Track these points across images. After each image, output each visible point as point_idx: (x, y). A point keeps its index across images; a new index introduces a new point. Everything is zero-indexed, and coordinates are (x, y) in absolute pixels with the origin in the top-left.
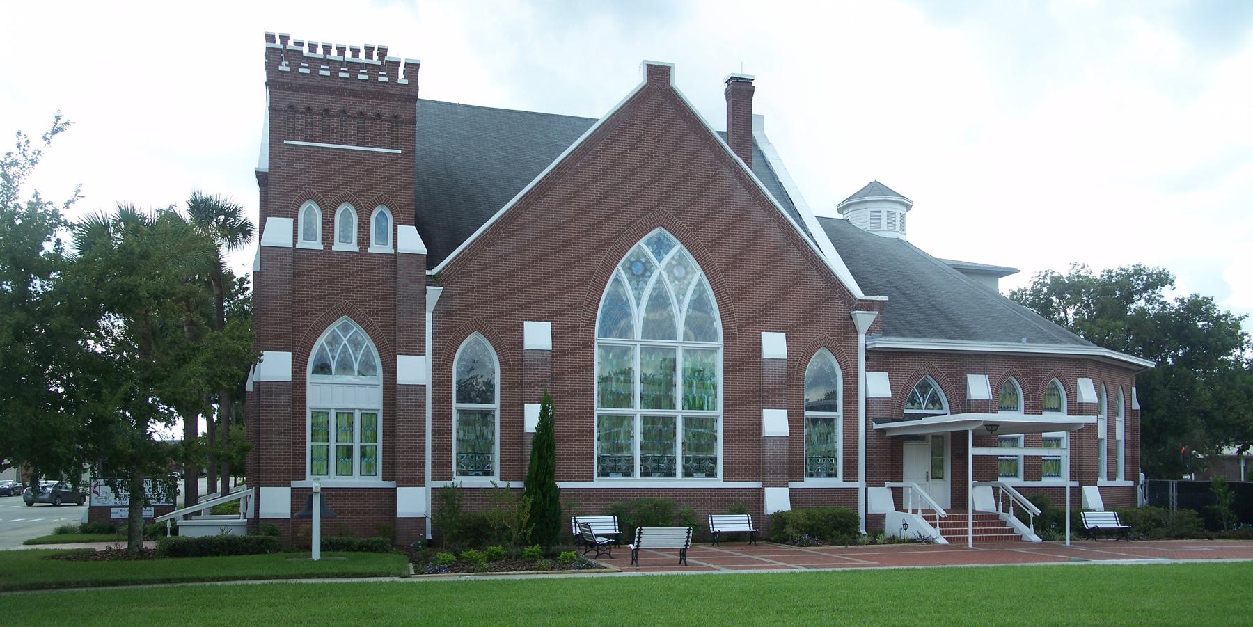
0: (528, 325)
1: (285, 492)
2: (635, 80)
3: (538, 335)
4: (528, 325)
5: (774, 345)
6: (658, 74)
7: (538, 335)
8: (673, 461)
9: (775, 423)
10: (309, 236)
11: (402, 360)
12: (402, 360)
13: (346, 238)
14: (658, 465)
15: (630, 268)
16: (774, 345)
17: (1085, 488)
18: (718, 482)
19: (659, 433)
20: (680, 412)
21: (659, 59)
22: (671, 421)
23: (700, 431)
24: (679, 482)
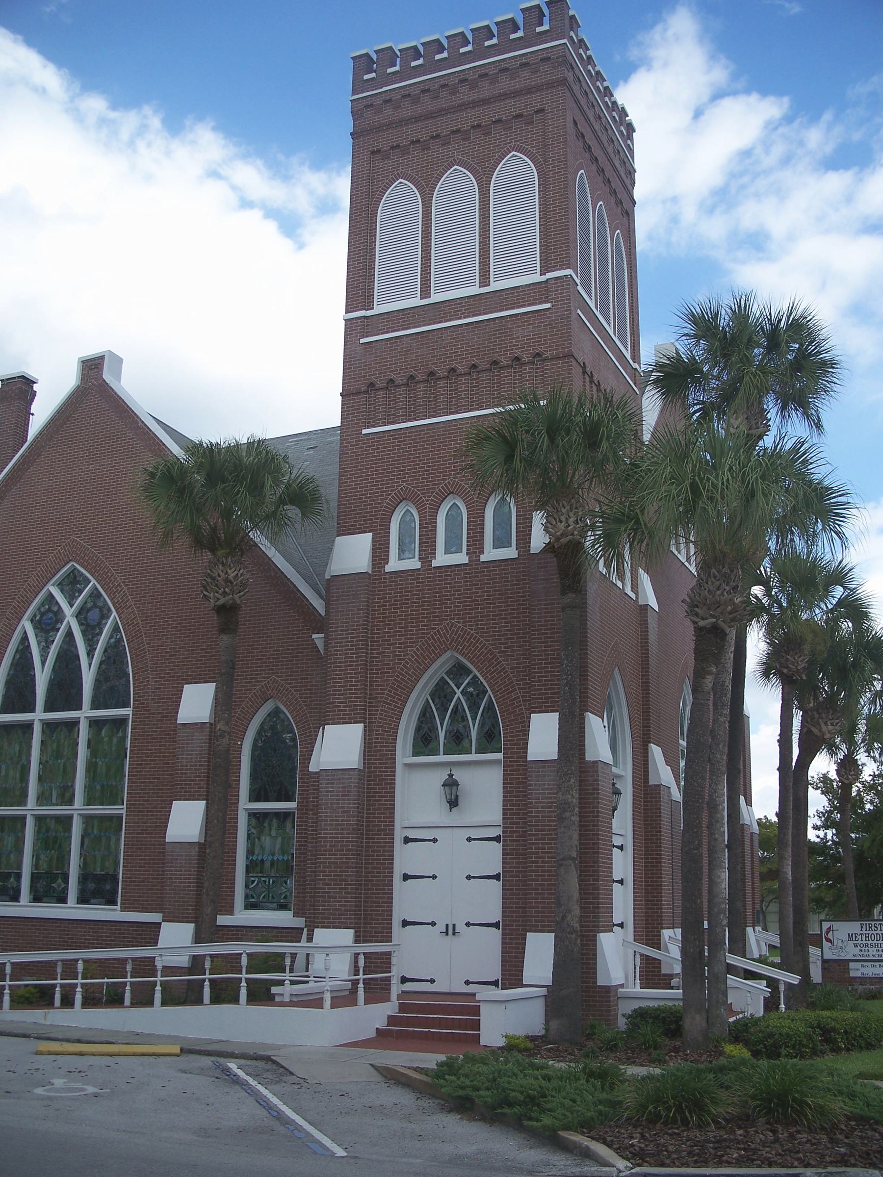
13: (499, 543)
15: (40, 621)
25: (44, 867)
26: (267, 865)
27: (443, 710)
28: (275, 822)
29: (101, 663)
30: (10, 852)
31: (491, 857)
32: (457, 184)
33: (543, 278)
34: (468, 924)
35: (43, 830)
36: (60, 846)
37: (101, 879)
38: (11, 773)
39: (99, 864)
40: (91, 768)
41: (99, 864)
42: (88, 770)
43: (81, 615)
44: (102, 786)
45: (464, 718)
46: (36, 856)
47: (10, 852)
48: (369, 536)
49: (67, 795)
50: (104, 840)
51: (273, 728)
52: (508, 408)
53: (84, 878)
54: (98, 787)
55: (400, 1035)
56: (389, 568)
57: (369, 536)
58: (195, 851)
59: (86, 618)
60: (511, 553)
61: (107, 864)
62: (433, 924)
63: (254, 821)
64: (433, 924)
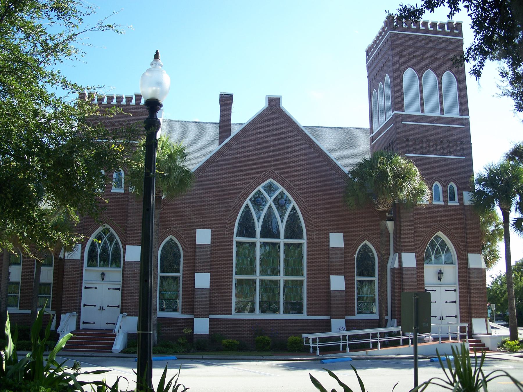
0: (332, 235)
1: (207, 320)
2: (262, 105)
3: (204, 236)
4: (332, 235)
5: (336, 240)
6: (274, 103)
7: (204, 236)
8: (278, 303)
9: (338, 283)
10: (452, 199)
11: (471, 256)
12: (471, 256)
13: (119, 186)
14: (294, 306)
15: (254, 201)
16: (336, 240)
17: (333, 321)
18: (304, 316)
19: (269, 288)
20: (258, 277)
21: (274, 94)
22: (277, 282)
23: (293, 287)
24: (281, 316)
25: (265, 299)
26: (365, 298)
27: (433, 249)
28: (367, 283)
29: (287, 221)
30: (247, 293)
31: (455, 296)
32: (429, 75)
33: (461, 117)
34: (447, 317)
35: (264, 285)
36: (273, 291)
37: (292, 304)
38: (245, 262)
39: (293, 298)
40: (286, 261)
41: (293, 298)
42: (285, 262)
43: (276, 201)
44: (292, 269)
45: (440, 253)
46: (261, 296)
47: (247, 293)
48: (464, 192)
49: (275, 271)
50: (294, 289)
51: (364, 251)
52: (101, 141)
53: (286, 303)
54: (290, 269)
55: (71, 347)
56: (112, 191)
57: (464, 192)
58: (344, 294)
59: (278, 202)
60: (456, 203)
61: (296, 298)
62: (436, 317)
63: (359, 283)
64: (436, 317)
